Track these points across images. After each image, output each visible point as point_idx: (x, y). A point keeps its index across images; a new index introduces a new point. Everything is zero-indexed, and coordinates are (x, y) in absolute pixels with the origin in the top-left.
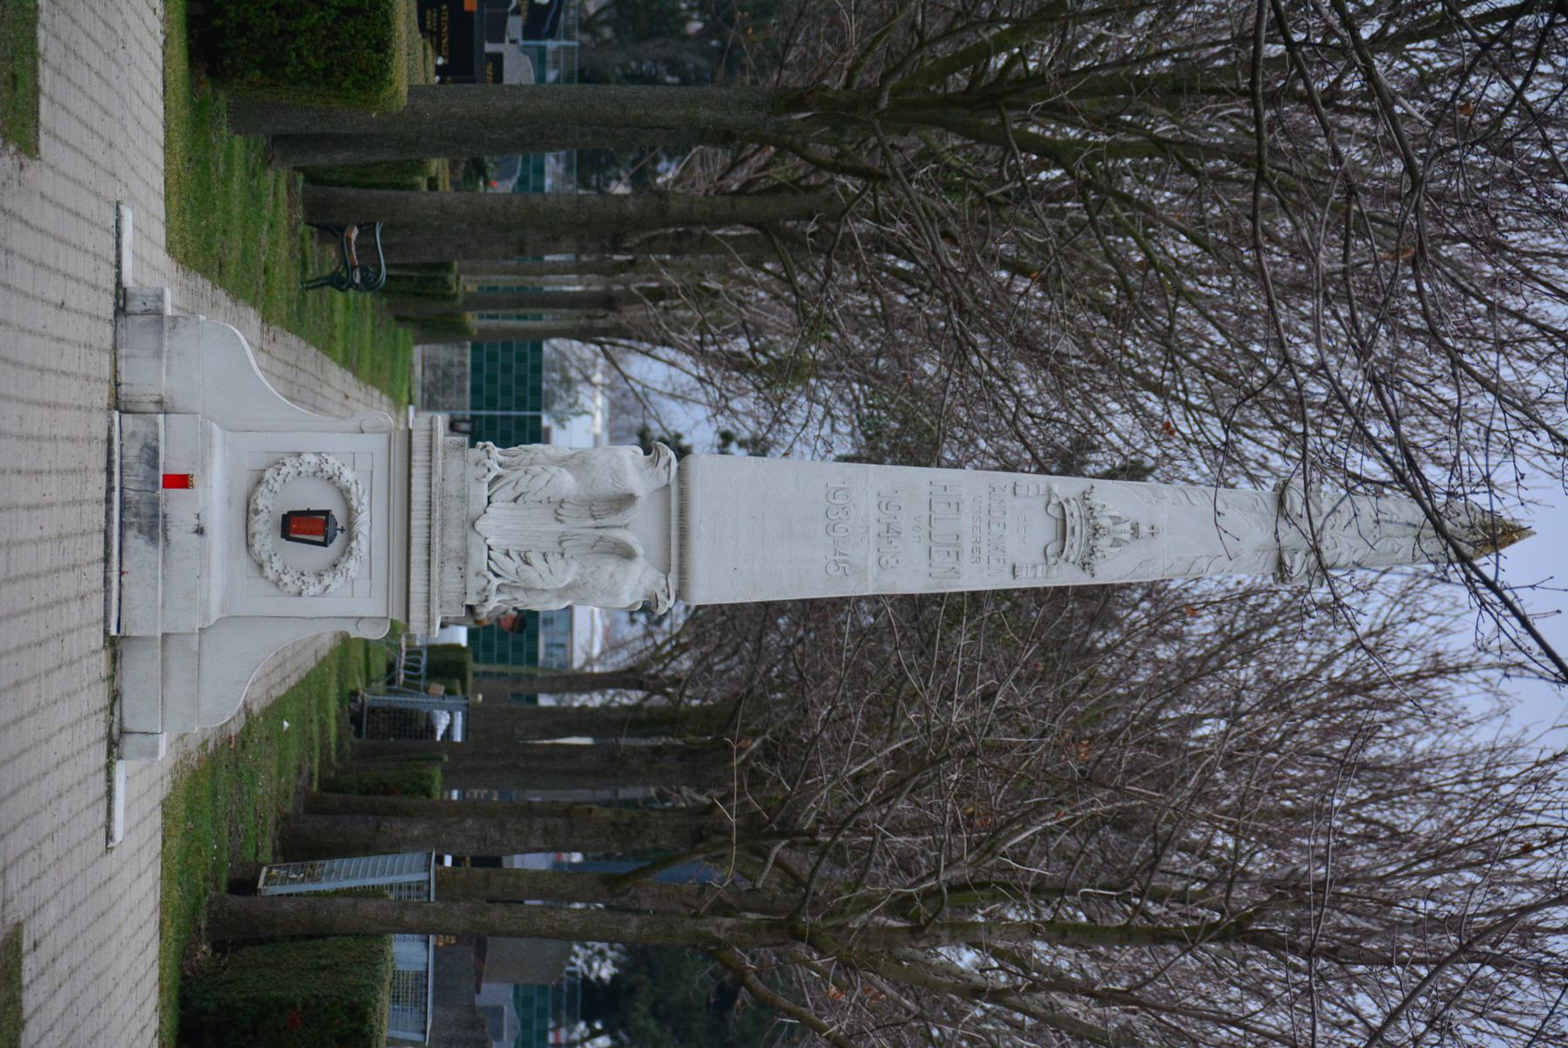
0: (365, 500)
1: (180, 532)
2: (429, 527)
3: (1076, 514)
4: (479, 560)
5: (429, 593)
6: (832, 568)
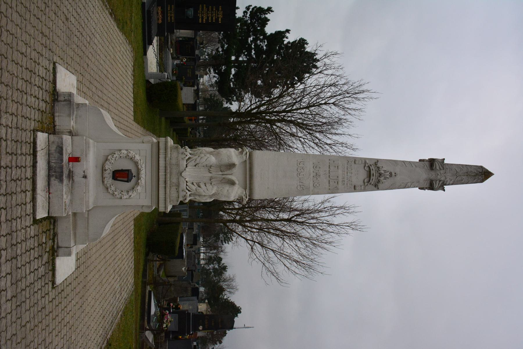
0: (143, 166)
1: (78, 178)
2: (165, 175)
4: (183, 186)
5: (165, 198)
6: (299, 187)
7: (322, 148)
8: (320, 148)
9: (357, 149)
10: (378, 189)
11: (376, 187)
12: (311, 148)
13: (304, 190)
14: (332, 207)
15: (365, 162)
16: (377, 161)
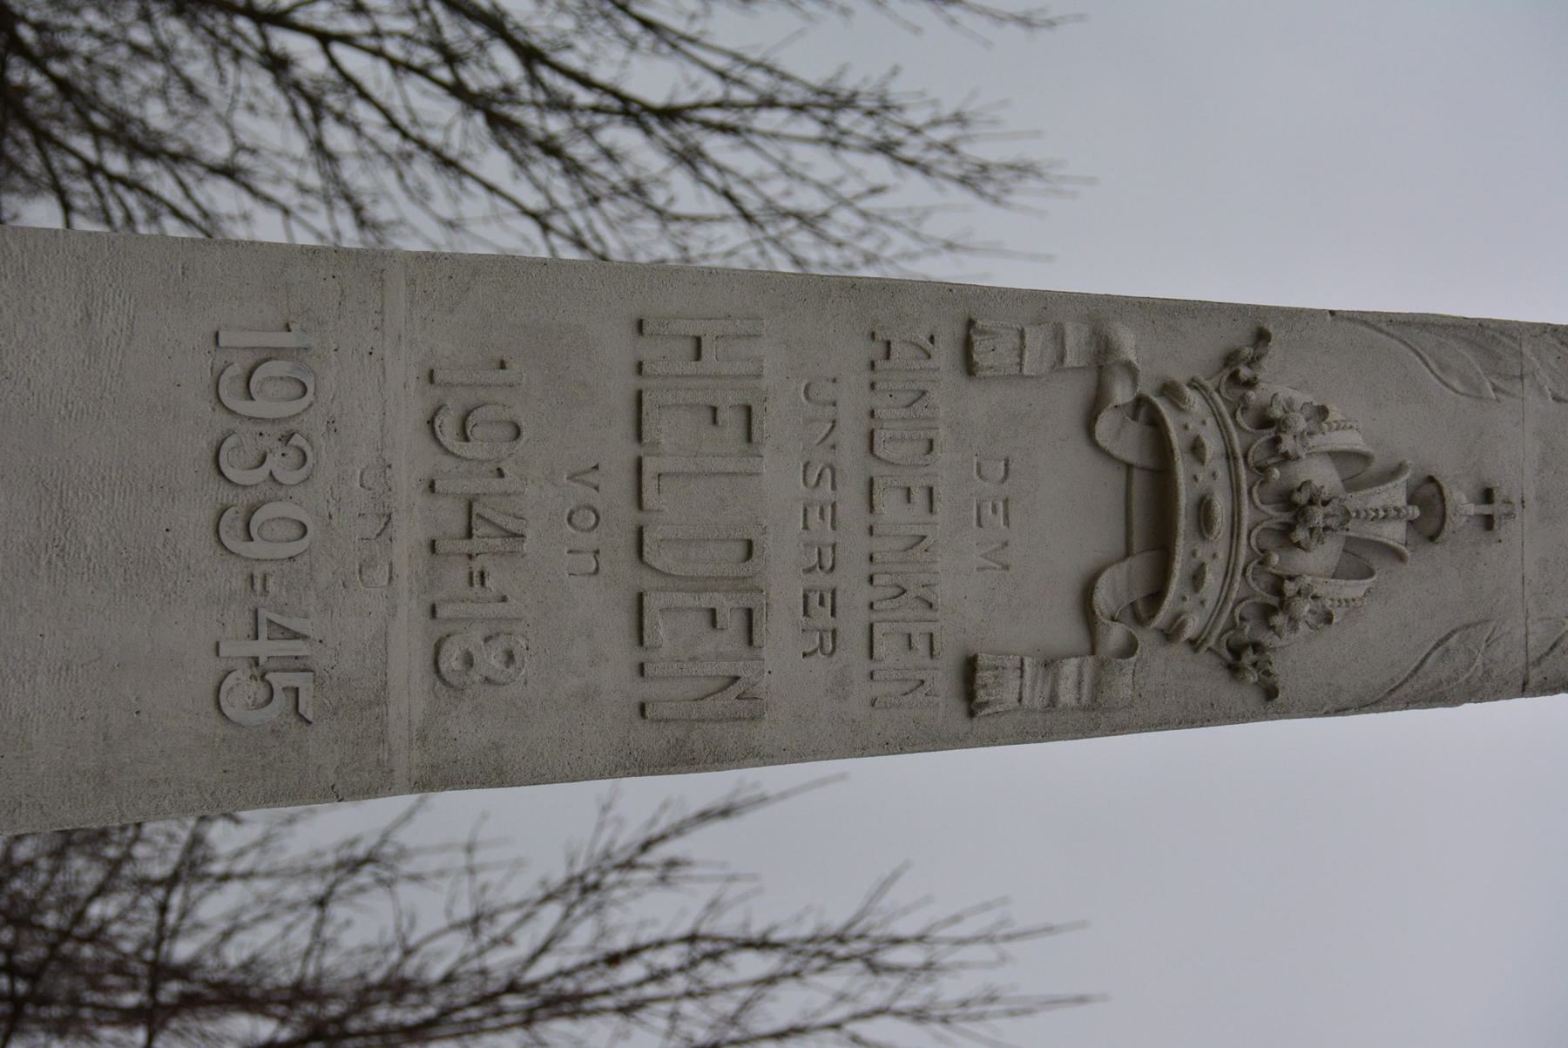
3: (1213, 446)
6: (241, 694)
7: (573, 169)
8: (546, 169)
9: (1022, 170)
10: (1270, 699)
11: (1248, 673)
12: (422, 169)
13: (311, 737)
14: (704, 947)
15: (1103, 355)
16: (1255, 335)
